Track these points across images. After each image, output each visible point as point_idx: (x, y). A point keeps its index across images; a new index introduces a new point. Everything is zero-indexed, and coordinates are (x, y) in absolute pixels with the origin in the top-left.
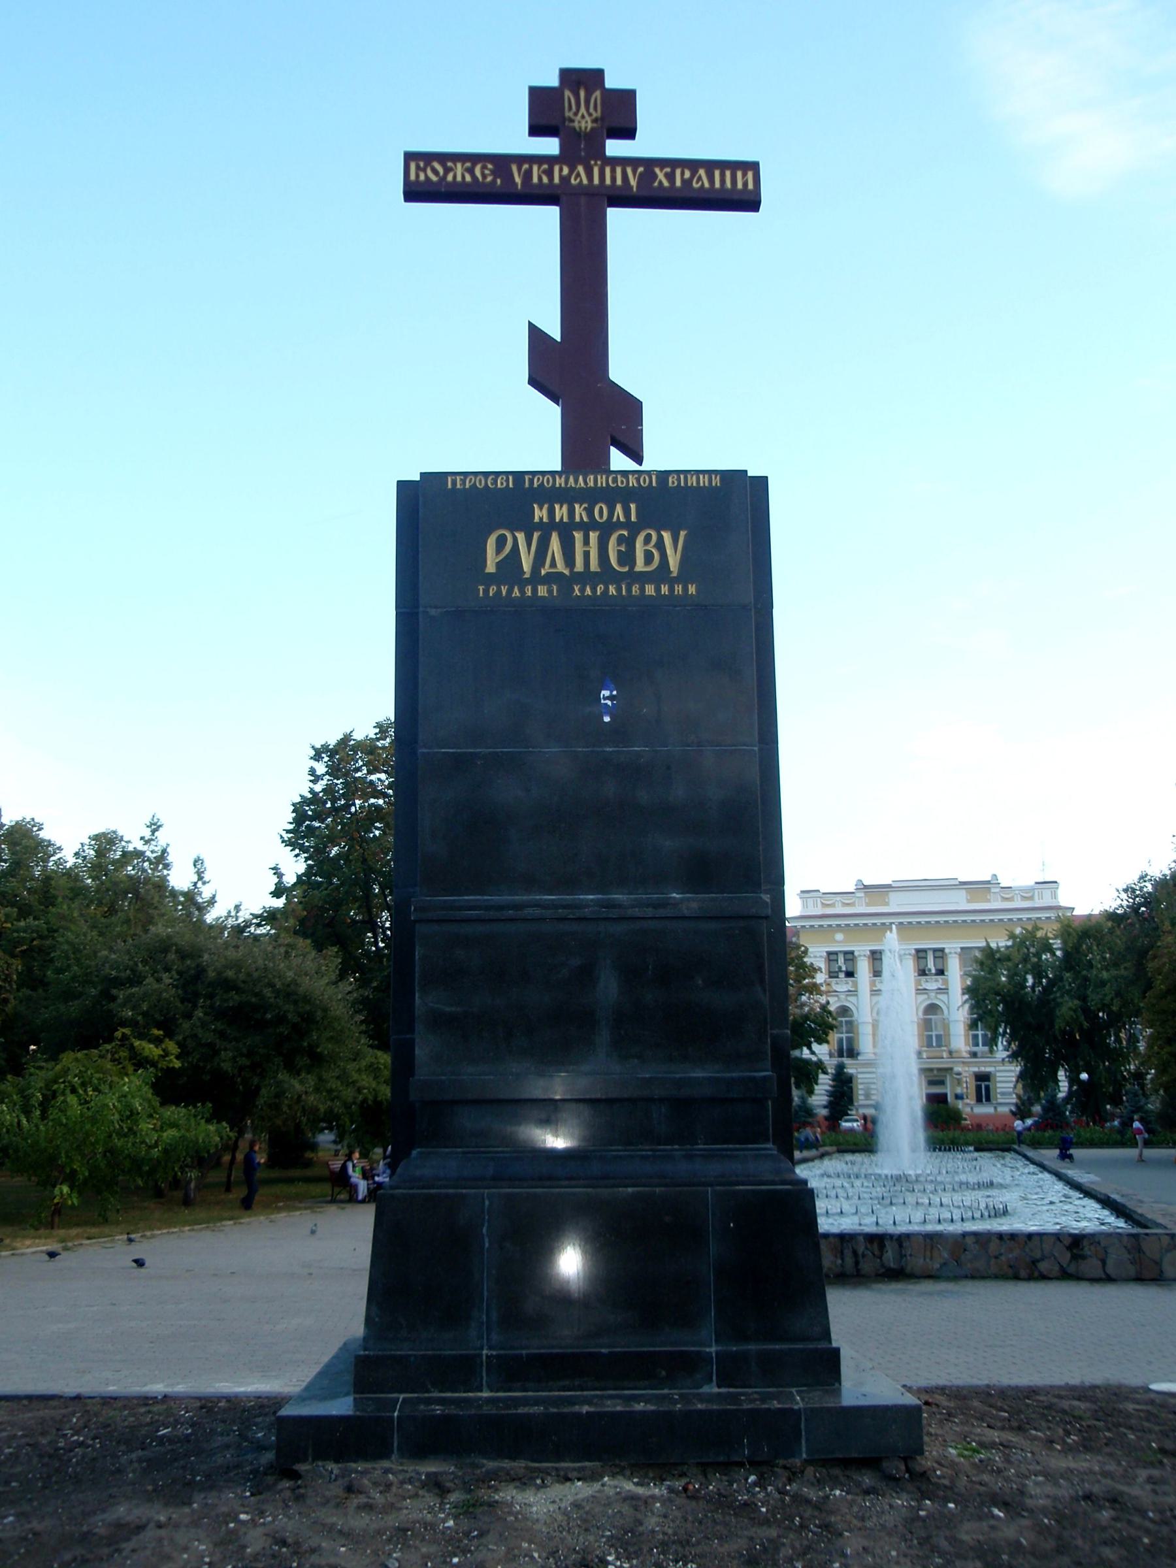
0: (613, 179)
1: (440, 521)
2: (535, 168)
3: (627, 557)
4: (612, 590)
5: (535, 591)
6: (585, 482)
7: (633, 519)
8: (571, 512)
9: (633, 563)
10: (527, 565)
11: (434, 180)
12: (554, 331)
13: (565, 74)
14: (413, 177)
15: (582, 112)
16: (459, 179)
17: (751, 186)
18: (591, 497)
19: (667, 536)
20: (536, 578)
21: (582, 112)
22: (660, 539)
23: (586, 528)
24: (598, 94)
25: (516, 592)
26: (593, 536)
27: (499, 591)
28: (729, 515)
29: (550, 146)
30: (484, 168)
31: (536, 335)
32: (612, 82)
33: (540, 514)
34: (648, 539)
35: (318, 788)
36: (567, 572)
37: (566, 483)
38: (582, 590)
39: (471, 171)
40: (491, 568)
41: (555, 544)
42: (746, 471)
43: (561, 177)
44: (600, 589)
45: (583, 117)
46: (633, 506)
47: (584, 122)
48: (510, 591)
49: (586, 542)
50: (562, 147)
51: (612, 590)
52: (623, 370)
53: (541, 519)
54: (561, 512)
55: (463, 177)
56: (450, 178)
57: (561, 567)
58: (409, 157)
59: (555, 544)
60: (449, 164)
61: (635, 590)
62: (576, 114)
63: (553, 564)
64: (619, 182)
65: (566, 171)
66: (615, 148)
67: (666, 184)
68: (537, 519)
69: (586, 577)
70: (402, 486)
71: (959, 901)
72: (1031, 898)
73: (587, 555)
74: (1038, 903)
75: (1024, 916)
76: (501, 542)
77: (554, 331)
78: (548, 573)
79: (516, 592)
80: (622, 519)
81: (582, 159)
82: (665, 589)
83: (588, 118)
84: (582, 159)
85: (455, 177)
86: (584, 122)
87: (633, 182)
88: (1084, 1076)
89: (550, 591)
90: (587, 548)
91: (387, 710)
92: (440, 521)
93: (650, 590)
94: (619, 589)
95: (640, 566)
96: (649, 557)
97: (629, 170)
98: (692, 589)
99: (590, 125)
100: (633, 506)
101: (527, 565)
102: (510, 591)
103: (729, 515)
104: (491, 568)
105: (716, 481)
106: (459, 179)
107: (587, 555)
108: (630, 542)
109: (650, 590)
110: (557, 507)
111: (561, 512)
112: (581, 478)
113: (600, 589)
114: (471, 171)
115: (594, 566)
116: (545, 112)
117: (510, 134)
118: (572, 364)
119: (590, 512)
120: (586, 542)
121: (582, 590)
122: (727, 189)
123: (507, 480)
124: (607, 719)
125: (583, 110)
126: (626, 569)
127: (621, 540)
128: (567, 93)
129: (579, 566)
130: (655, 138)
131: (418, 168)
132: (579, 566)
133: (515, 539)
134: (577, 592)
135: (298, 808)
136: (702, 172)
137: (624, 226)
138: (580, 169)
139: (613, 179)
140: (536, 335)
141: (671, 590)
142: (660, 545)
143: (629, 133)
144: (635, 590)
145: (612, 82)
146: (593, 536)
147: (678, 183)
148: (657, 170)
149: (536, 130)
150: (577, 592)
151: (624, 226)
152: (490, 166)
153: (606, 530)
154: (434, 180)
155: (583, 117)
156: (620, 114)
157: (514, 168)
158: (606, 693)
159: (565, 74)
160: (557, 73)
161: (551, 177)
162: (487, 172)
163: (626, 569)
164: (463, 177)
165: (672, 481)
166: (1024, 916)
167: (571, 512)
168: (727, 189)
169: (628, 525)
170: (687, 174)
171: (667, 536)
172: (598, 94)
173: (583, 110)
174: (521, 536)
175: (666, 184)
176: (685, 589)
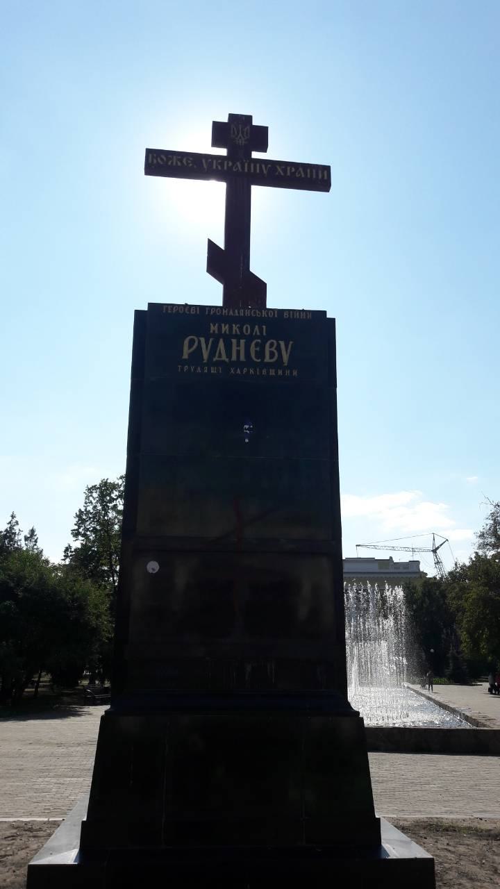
0: (255, 169)
1: (158, 330)
2: (215, 162)
3: (261, 354)
4: (252, 371)
5: (209, 370)
6: (239, 313)
7: (264, 334)
8: (231, 328)
9: (263, 357)
10: (206, 355)
11: (162, 163)
12: (221, 243)
13: (232, 116)
14: (150, 161)
15: (240, 135)
16: (174, 164)
17: (326, 178)
18: (242, 321)
19: (282, 344)
20: (210, 363)
21: (240, 135)
22: (279, 346)
23: (238, 338)
24: (248, 127)
25: (199, 370)
26: (242, 342)
27: (190, 369)
28: (313, 335)
29: (223, 152)
30: (188, 159)
31: (212, 245)
32: (255, 122)
33: (214, 328)
34: (272, 345)
35: (90, 508)
36: (227, 360)
37: (228, 313)
38: (235, 371)
39: (181, 161)
40: (185, 356)
41: (221, 345)
42: (325, 312)
43: (228, 167)
44: (245, 370)
45: (240, 138)
46: (264, 327)
47: (241, 141)
48: (195, 369)
49: (238, 345)
50: (228, 153)
51: (252, 371)
52: (257, 267)
53: (214, 331)
54: (225, 328)
55: (177, 163)
56: (170, 163)
57: (224, 358)
58: (149, 152)
59: (221, 345)
60: (170, 156)
61: (264, 372)
62: (237, 136)
63: (220, 356)
64: (258, 171)
65: (230, 164)
66: (256, 155)
67: (282, 174)
68: (211, 331)
69: (238, 364)
70: (138, 313)
71: (375, 568)
72: (408, 568)
73: (238, 352)
74: (410, 570)
75: (404, 576)
76: (191, 343)
77: (221, 243)
78: (217, 361)
79: (199, 370)
80: (258, 334)
81: (240, 156)
82: (280, 372)
83: (243, 139)
84: (240, 156)
85: (172, 163)
86: (241, 141)
87: (265, 172)
88: (432, 650)
89: (218, 370)
90: (238, 348)
91: (123, 471)
92: (158, 330)
93: (272, 372)
94: (255, 371)
95: (267, 359)
96: (272, 355)
97: (263, 166)
98: (295, 373)
99: (243, 142)
100: (264, 327)
101: (206, 355)
102: (195, 369)
103: (313, 335)
104: (185, 356)
105: (309, 316)
106: (174, 164)
107: (238, 352)
108: (262, 346)
109: (272, 372)
110: (223, 325)
111: (225, 328)
112: (236, 311)
113: (245, 370)
114: (181, 161)
115: (242, 358)
116: (221, 133)
117: (201, 143)
118: (230, 260)
119: (241, 329)
120: (238, 345)
121: (235, 371)
122: (313, 178)
123: (196, 310)
124: (247, 441)
125: (240, 135)
126: (259, 360)
127: (257, 345)
128: (232, 126)
129: (234, 358)
130: (277, 151)
131: (153, 157)
132: (234, 358)
133: (199, 342)
134: (232, 371)
135: (80, 515)
136: (301, 169)
137: (260, 195)
138: (238, 164)
139: (255, 169)
140: (212, 245)
141: (284, 372)
142: (278, 348)
143: (263, 147)
144: (264, 372)
145: (255, 122)
146: (242, 342)
147: (289, 174)
148: (278, 167)
149: (216, 142)
150: (232, 371)
151: (260, 195)
152: (191, 159)
153: (249, 339)
154: (162, 163)
155: (240, 138)
156: (260, 137)
157: (204, 161)
158: (247, 427)
159: (232, 116)
160: (227, 116)
161: (223, 167)
162: (189, 162)
163: (259, 360)
164: (177, 163)
165: (286, 315)
166: (404, 576)
167: (231, 328)
168: (313, 178)
169: (261, 337)
170: (293, 170)
171: (282, 344)
172: (248, 127)
173: (240, 135)
174: (202, 340)
175: (282, 174)
176: (291, 373)
